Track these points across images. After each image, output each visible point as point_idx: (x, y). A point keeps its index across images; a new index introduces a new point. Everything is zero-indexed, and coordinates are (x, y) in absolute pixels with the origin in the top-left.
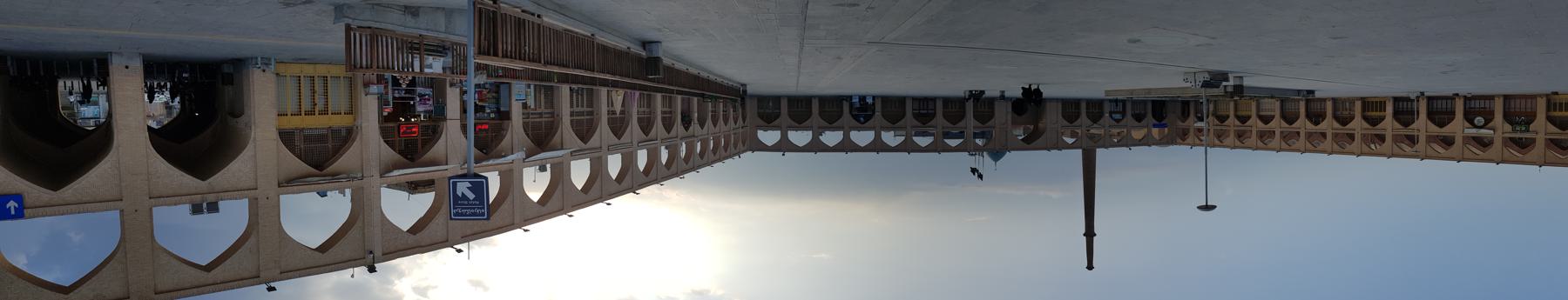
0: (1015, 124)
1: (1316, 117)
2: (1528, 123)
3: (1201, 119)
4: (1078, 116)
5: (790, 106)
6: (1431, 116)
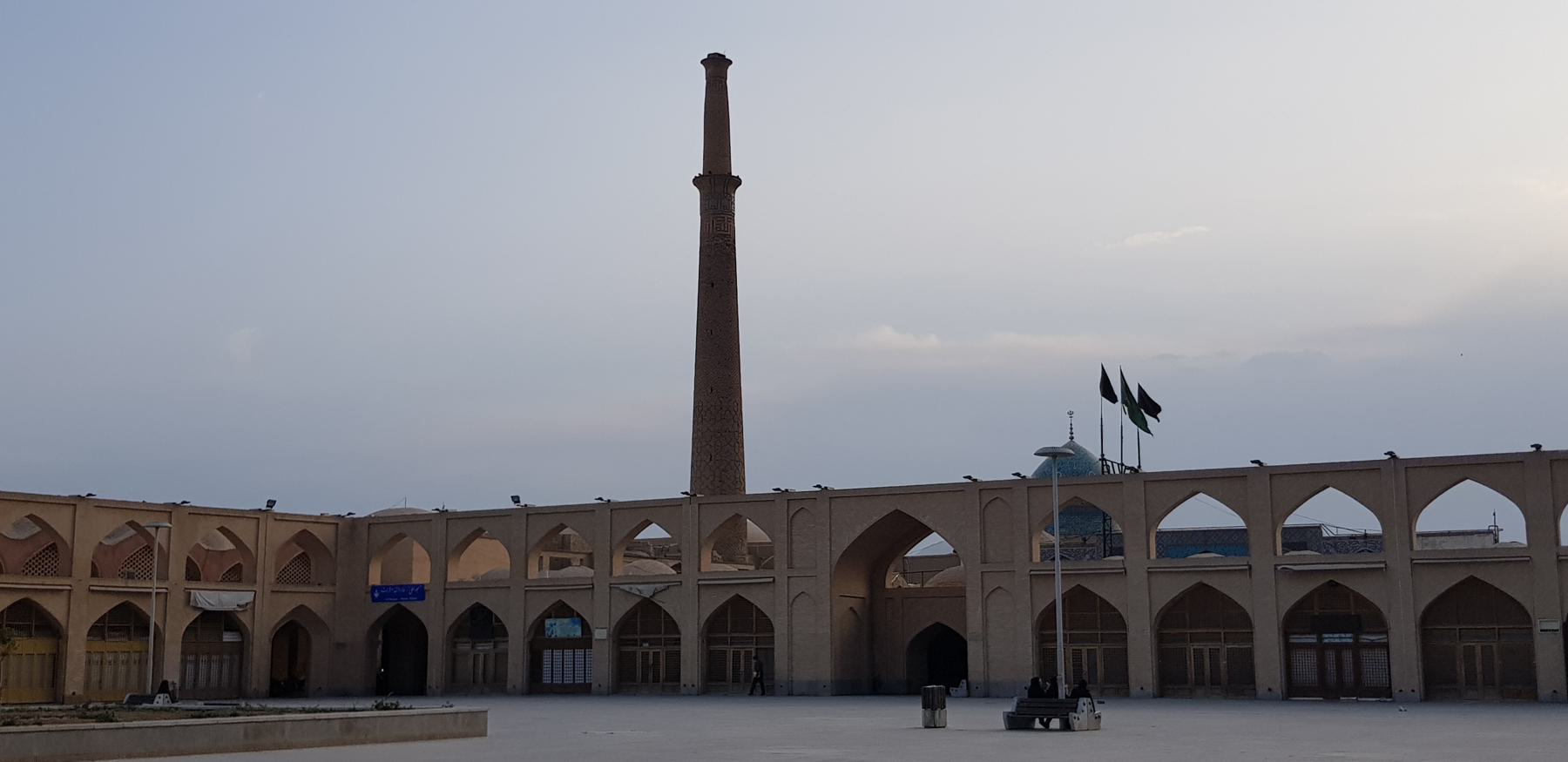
4: (714, 627)
5: (674, 659)
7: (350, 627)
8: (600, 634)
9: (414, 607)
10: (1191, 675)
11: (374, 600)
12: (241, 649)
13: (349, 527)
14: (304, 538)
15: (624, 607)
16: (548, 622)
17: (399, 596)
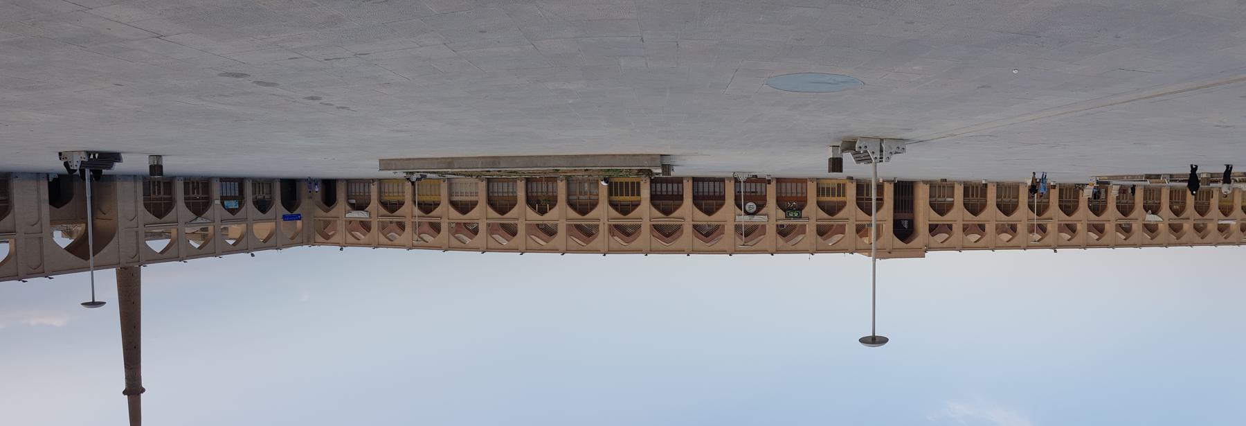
0: (55, 222)
1: (540, 204)
2: (800, 209)
3: (360, 207)
4: (170, 205)
6: (697, 200)
7: (309, 204)
8: (218, 202)
9: (287, 213)
12: (348, 197)
13: (310, 241)
14: (327, 237)
15: (209, 213)
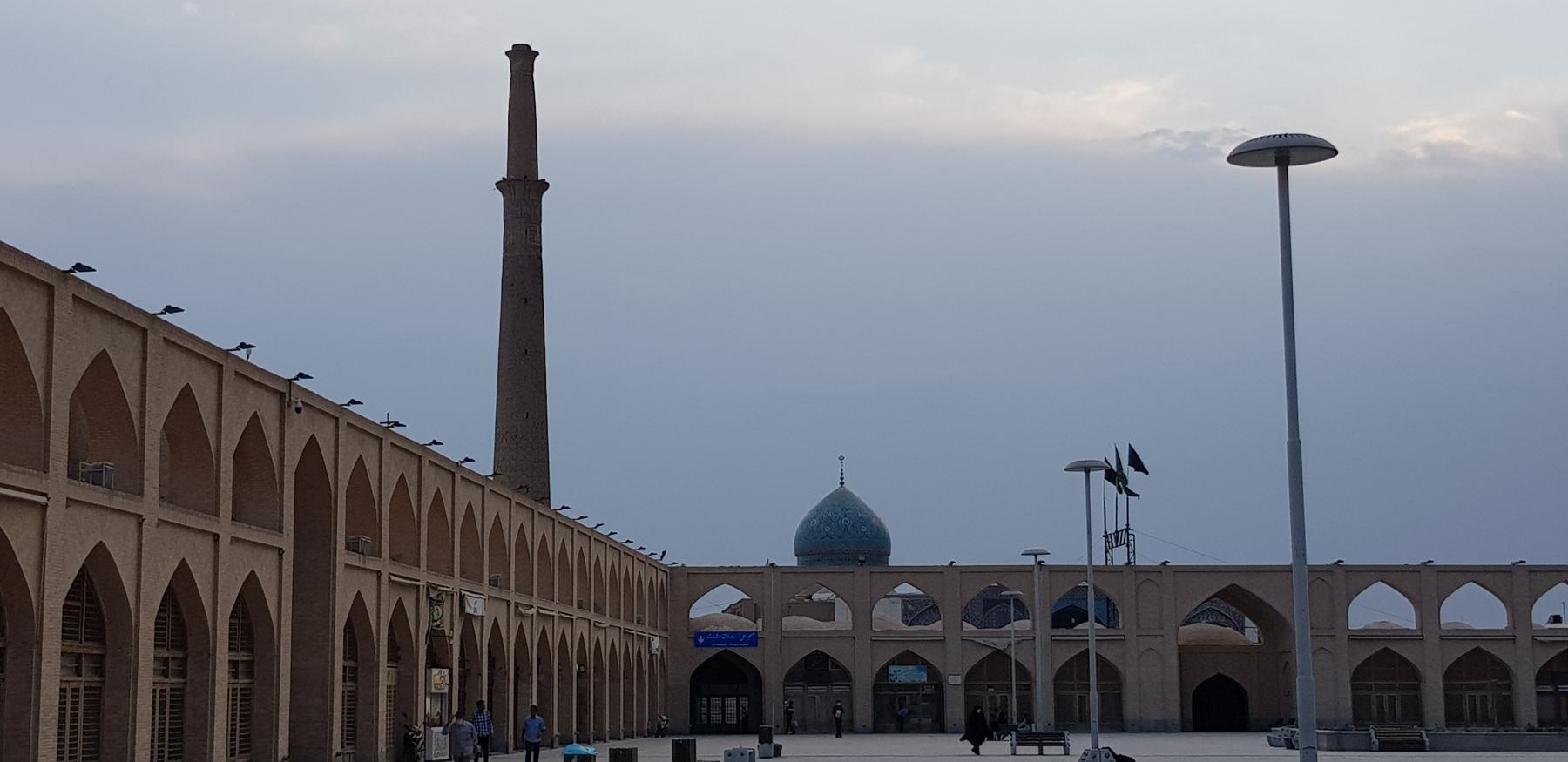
10: (1467, 716)
11: (697, 645)
16: (892, 669)
17: (728, 642)
